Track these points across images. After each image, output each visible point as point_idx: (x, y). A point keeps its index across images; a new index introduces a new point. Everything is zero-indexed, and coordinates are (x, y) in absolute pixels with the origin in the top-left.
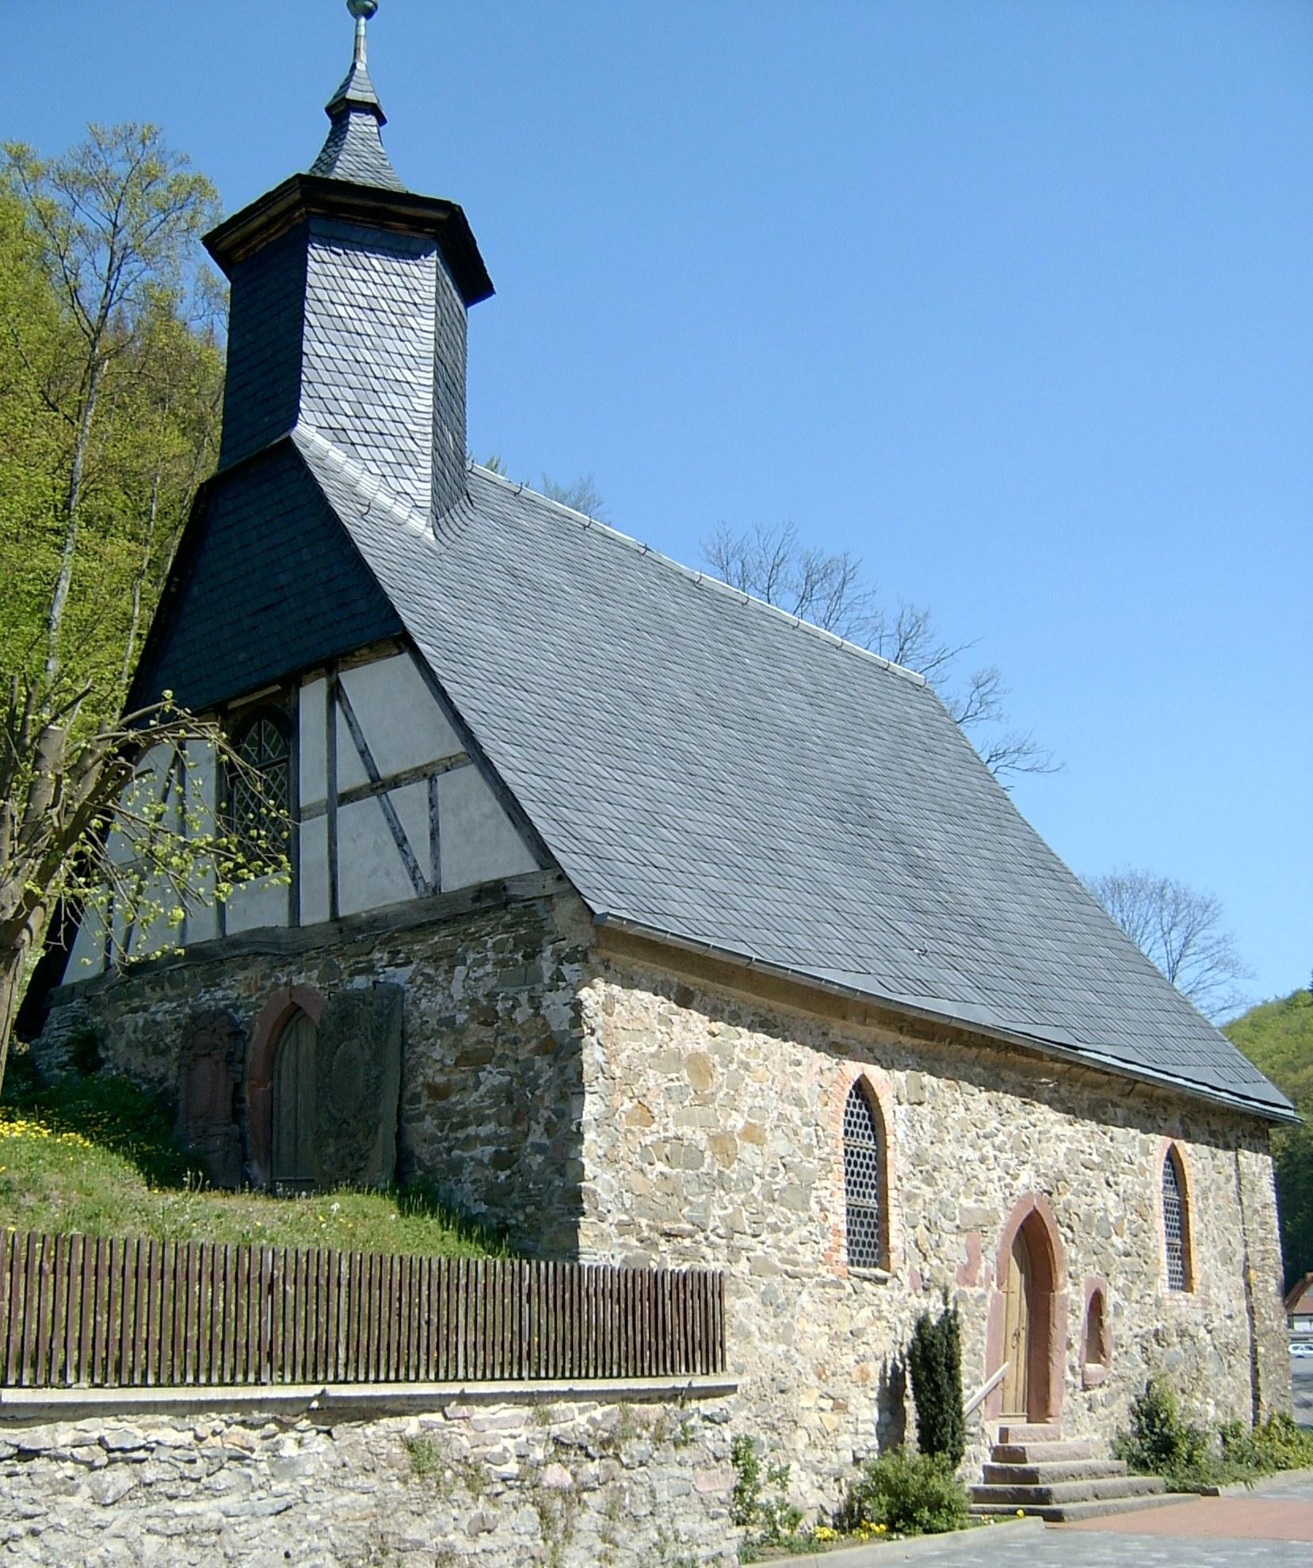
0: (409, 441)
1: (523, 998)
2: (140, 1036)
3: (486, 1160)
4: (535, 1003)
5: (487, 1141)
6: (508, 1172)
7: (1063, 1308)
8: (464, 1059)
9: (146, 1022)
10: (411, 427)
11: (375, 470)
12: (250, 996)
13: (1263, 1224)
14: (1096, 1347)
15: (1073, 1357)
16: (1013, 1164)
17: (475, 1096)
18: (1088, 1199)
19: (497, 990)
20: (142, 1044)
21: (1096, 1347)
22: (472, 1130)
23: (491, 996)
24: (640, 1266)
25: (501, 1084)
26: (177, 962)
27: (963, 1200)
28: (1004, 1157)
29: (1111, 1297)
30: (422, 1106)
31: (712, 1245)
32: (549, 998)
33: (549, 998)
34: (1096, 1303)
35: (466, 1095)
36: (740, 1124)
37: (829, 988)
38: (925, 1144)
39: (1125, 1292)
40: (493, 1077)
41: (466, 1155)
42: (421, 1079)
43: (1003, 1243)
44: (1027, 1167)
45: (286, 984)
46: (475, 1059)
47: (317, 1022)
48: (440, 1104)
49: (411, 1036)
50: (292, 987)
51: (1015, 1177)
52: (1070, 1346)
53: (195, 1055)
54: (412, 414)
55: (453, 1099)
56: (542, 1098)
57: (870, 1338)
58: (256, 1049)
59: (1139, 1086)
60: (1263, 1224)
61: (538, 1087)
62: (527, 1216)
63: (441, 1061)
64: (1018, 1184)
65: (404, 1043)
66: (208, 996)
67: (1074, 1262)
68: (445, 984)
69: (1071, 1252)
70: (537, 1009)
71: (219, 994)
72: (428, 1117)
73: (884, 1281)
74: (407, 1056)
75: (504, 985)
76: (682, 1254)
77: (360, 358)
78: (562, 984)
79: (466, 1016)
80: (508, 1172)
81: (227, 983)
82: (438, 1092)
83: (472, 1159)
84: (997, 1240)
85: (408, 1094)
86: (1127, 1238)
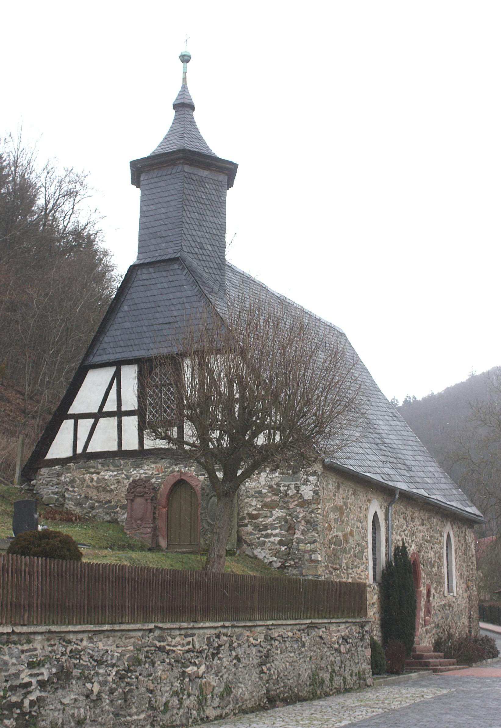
0: (218, 259)
1: (292, 487)
2: (95, 484)
3: (276, 542)
4: (297, 488)
5: (275, 536)
6: (286, 547)
7: (421, 595)
8: (265, 505)
9: (98, 478)
10: (219, 254)
11: (207, 271)
12: (159, 474)
13: (472, 563)
14: (428, 612)
15: (422, 614)
16: (410, 541)
17: (270, 519)
19: (281, 482)
20: (97, 487)
21: (428, 612)
22: (269, 531)
23: (278, 485)
24: (329, 580)
25: (282, 516)
29: (433, 591)
30: (246, 521)
31: (343, 573)
32: (303, 488)
33: (303, 488)
35: (266, 519)
37: (431, 503)
39: (436, 589)
40: (278, 513)
41: (267, 540)
42: (246, 512)
45: (178, 471)
46: (270, 506)
48: (254, 521)
49: (241, 496)
50: (182, 473)
53: (135, 495)
54: (220, 248)
55: (261, 520)
56: (300, 522)
59: (441, 510)
60: (472, 563)
61: (299, 518)
62: (295, 563)
63: (256, 506)
65: (238, 498)
66: (135, 472)
67: (424, 578)
68: (256, 478)
70: (298, 491)
71: (142, 471)
72: (249, 526)
74: (239, 503)
75: (282, 481)
76: (337, 576)
77: (201, 224)
78: (309, 483)
79: (267, 491)
80: (286, 547)
81: (146, 468)
82: (252, 517)
83: (269, 542)
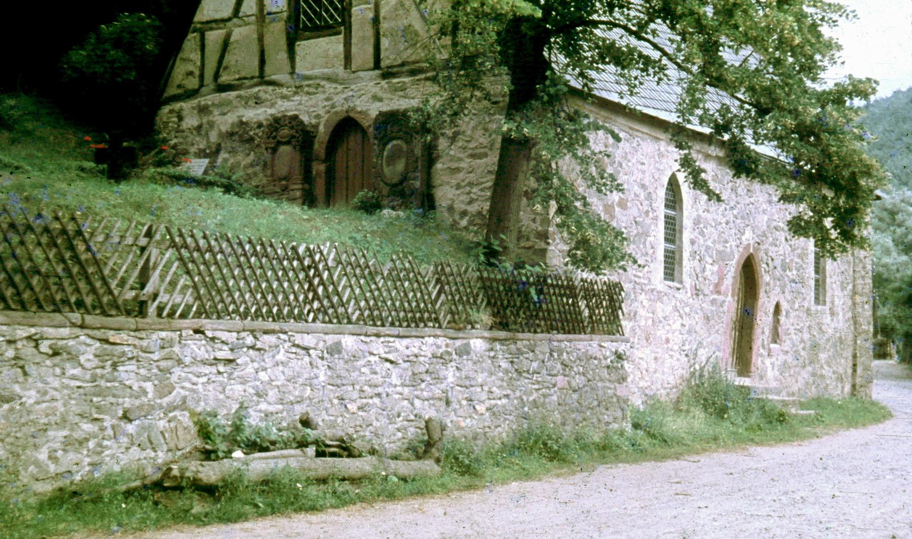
14: (776, 337)
18: (776, 249)
21: (776, 337)
26: (407, 71)
27: (717, 246)
28: (738, 221)
29: (784, 306)
34: (777, 308)
36: (617, 199)
38: (701, 212)
43: (735, 272)
44: (749, 228)
47: (49, 379)
51: (743, 234)
52: (763, 332)
57: (671, 322)
58: (319, 147)
64: (744, 238)
69: (767, 278)
73: (678, 289)
84: (733, 270)
85: (224, 64)
86: (795, 272)
